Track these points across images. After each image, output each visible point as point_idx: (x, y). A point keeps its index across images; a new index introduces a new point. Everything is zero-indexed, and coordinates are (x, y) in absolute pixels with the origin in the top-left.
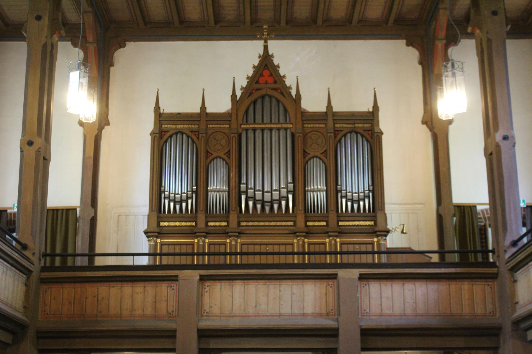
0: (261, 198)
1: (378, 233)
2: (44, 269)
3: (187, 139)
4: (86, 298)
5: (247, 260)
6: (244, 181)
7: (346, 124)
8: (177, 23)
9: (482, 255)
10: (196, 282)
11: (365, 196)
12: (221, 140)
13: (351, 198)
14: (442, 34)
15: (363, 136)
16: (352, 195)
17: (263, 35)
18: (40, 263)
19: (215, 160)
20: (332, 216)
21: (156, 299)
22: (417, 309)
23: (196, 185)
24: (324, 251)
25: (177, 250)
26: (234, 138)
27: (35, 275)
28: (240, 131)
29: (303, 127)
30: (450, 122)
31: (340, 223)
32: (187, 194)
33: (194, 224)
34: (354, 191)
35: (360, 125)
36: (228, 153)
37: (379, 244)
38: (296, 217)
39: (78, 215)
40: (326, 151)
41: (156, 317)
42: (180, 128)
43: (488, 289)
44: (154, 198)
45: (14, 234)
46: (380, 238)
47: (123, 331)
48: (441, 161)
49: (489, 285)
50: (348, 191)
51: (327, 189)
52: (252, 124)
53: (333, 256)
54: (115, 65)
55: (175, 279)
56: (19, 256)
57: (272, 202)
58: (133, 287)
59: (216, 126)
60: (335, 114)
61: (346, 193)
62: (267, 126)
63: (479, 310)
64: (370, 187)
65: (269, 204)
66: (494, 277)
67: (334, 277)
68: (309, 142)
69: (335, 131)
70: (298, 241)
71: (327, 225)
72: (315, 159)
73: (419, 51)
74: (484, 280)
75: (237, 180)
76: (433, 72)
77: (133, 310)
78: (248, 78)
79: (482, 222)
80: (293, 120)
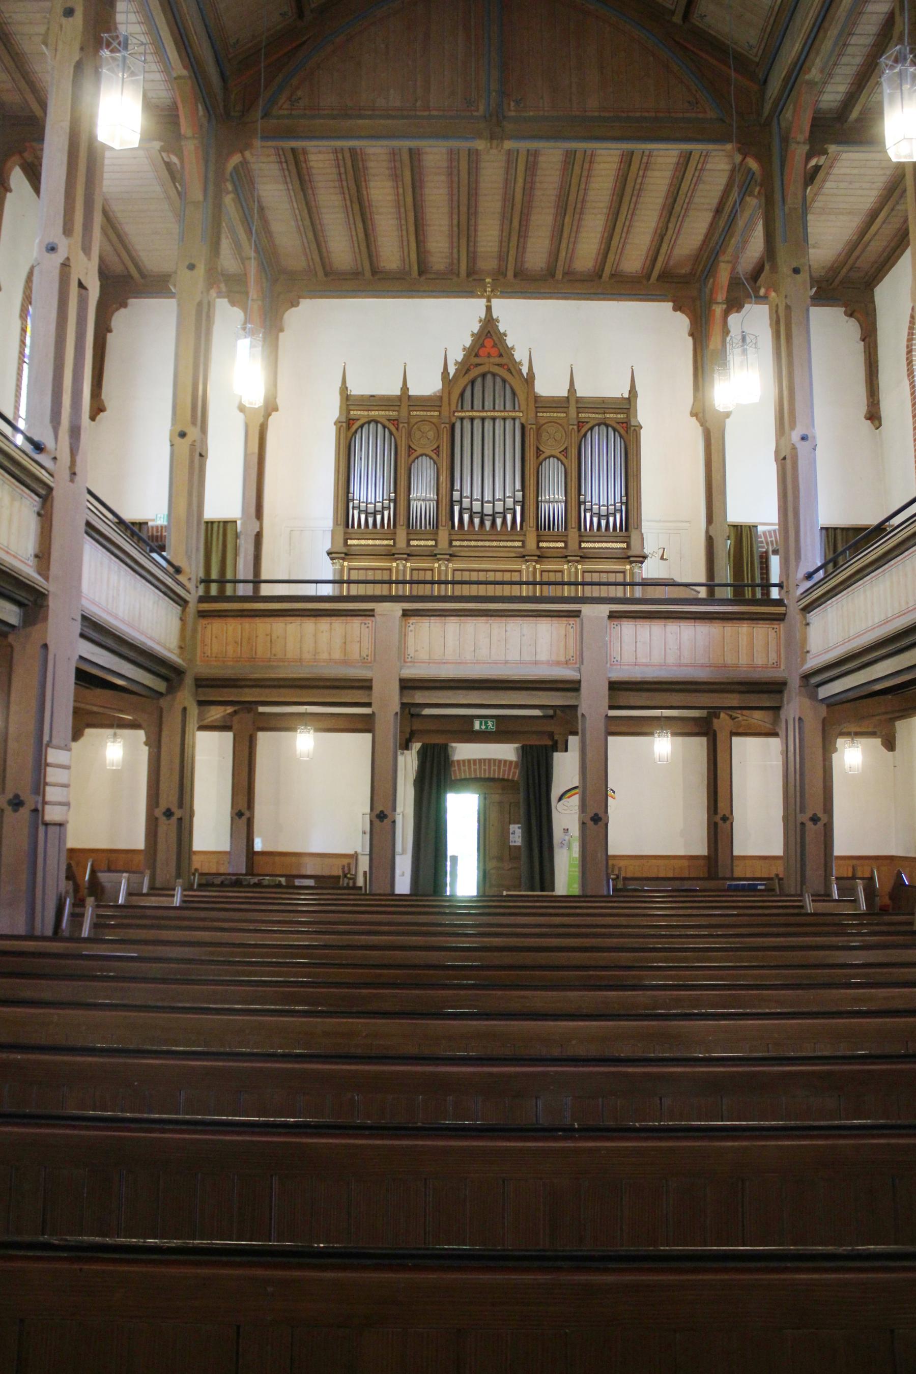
0: (479, 510)
1: (632, 559)
2: (202, 600)
3: (382, 430)
4: (257, 637)
5: (459, 590)
6: (457, 486)
7: (593, 413)
8: (368, 274)
9: (762, 590)
10: (398, 619)
11: (383, 508)
13: (597, 512)
14: (721, 296)
15: (615, 430)
16: (599, 508)
17: (486, 291)
18: (197, 591)
19: (420, 458)
20: (573, 534)
21: (345, 639)
22: (682, 658)
23: (395, 492)
24: (430, 579)
25: (370, 576)
26: (445, 429)
27: (192, 607)
28: (453, 420)
29: (537, 416)
30: (728, 415)
31: (583, 545)
32: (383, 503)
33: (391, 542)
34: (601, 504)
35: (612, 416)
36: (437, 450)
37: (632, 574)
38: (525, 535)
39: (239, 529)
40: (566, 448)
41: (345, 662)
43: (772, 634)
44: (339, 509)
45: (164, 553)
46: (634, 565)
47: (300, 679)
48: (715, 466)
49: (773, 629)
50: (594, 503)
51: (566, 500)
52: (468, 411)
53: (573, 587)
54: (285, 329)
55: (370, 614)
56: (173, 583)
57: (494, 516)
58: (316, 623)
59: (422, 413)
60: (579, 400)
61: (592, 505)
62: (489, 414)
63: (759, 661)
65: (490, 518)
66: (781, 618)
67: (576, 614)
68: (545, 436)
69: (579, 422)
70: (528, 568)
71: (566, 547)
72: (551, 459)
73: (689, 318)
74: (767, 622)
75: (449, 486)
76: (707, 346)
77: (316, 653)
78: (464, 349)
79: (763, 547)
80: (523, 408)
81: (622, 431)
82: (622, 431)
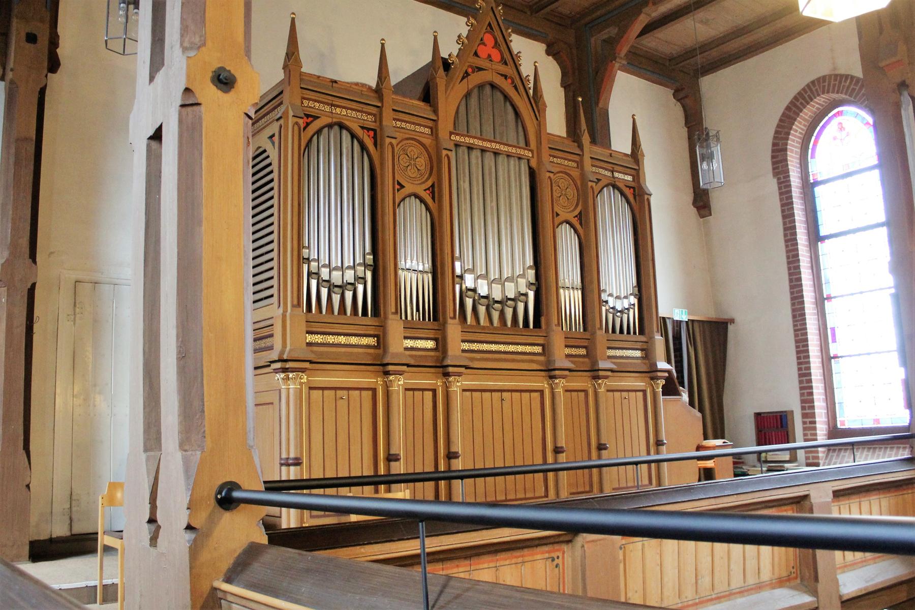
11: (357, 278)
12: (417, 158)
15: (353, 136)
50: (322, 263)
64: (368, 257)
81: (369, 143)
82: (369, 143)
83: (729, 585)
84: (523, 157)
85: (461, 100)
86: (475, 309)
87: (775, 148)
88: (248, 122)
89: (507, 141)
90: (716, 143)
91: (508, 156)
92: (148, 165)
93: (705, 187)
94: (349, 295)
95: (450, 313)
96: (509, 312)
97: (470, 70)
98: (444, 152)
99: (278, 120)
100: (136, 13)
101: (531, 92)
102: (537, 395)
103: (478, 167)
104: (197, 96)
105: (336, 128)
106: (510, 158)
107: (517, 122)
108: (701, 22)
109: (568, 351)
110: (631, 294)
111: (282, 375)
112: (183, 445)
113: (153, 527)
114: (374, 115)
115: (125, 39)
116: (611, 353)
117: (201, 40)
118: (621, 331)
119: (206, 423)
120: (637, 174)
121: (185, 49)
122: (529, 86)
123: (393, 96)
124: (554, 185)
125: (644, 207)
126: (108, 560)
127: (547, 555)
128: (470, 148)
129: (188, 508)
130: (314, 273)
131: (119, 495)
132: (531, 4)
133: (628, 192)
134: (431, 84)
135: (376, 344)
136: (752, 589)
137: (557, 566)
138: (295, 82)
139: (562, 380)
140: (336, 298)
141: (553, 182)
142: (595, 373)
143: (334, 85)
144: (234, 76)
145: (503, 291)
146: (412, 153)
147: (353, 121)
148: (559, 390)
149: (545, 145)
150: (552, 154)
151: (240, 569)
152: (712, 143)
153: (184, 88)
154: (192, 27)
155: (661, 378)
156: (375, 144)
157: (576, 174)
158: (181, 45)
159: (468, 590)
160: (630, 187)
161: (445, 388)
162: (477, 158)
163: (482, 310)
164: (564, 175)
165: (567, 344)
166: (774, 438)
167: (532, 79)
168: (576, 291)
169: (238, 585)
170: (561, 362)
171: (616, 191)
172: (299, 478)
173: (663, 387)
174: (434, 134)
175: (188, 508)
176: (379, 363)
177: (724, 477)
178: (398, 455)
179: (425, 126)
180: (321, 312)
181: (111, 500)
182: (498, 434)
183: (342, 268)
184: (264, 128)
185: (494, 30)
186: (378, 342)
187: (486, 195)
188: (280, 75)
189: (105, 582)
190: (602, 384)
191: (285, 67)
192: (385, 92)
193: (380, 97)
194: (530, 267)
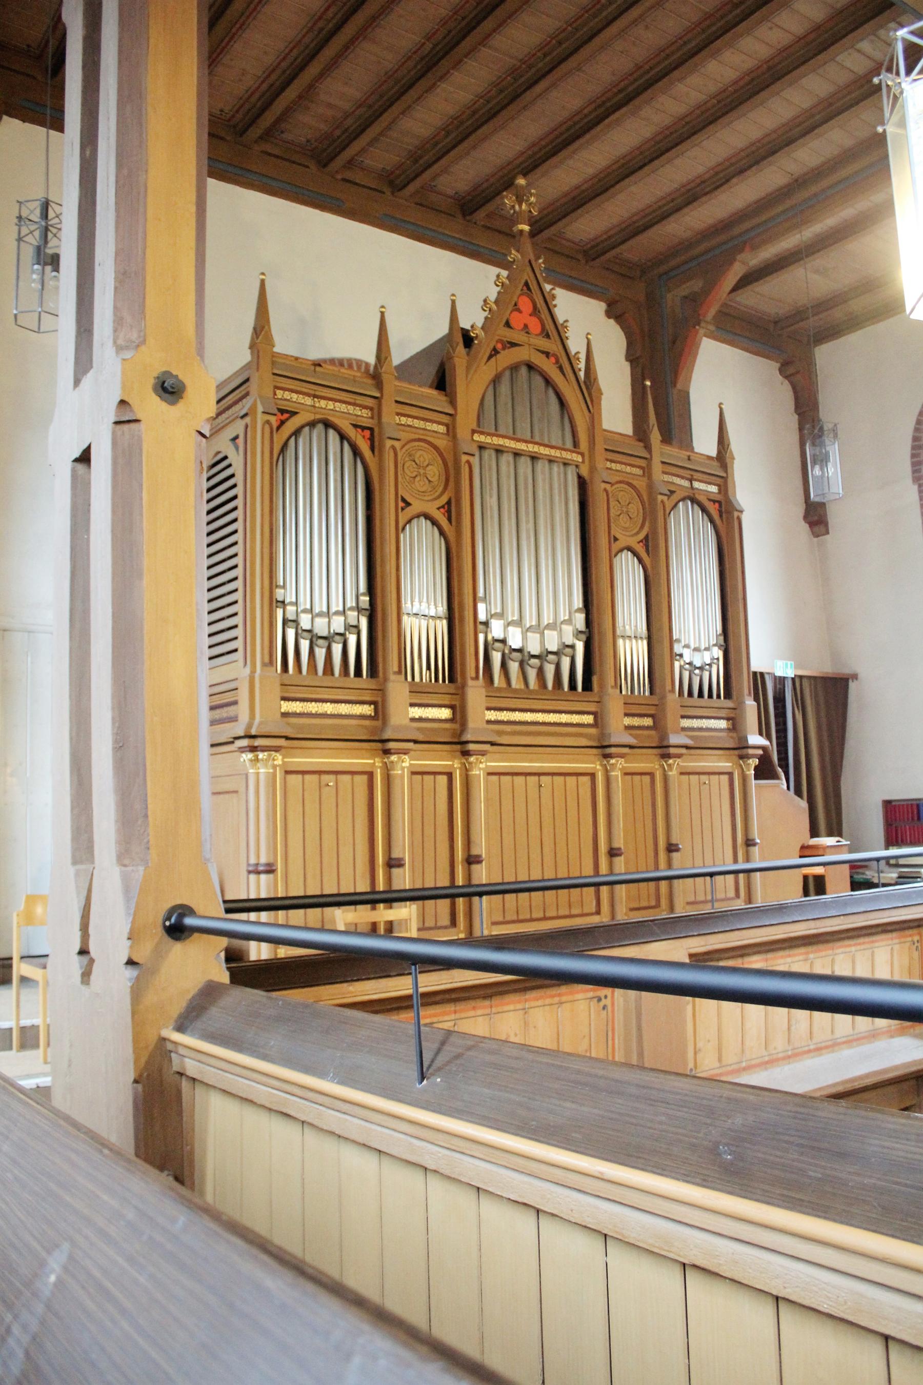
11: (348, 627)
12: (427, 466)
15: (343, 437)
19: (415, 521)
42: (325, 409)
50: (301, 608)
81: (364, 446)
82: (364, 446)
83: (832, 1032)
84: (571, 462)
85: (487, 387)
86: (504, 665)
87: (917, 443)
88: (201, 441)
89: (549, 441)
90: (832, 440)
91: (550, 461)
92: (74, 495)
93: (817, 499)
94: (337, 649)
95: (471, 672)
96: (550, 670)
97: (499, 346)
98: (464, 458)
99: (242, 417)
100: (55, 277)
101: (582, 374)
102: (586, 780)
103: (509, 477)
104: (135, 410)
105: (320, 427)
106: (552, 464)
107: (562, 417)
108: (817, 271)
109: (628, 721)
110: (714, 645)
111: (250, 756)
112: (123, 857)
113: (85, 959)
114: (371, 409)
115: (40, 313)
116: (686, 723)
117: (139, 337)
118: (701, 695)
119: (151, 830)
120: (724, 483)
121: (119, 349)
122: (579, 366)
123: (397, 383)
124: (611, 500)
125: (733, 527)
126: (25, 993)
127: (591, 994)
128: (499, 451)
129: (129, 939)
130: (291, 621)
131: (39, 910)
132: (585, 248)
133: (713, 509)
134: (447, 367)
135: (373, 714)
136: (863, 1038)
137: (604, 1007)
138: (265, 365)
139: (621, 761)
140: (320, 653)
141: (610, 495)
142: (664, 751)
143: (318, 369)
144: (183, 383)
145: (542, 642)
146: (422, 459)
147: (344, 418)
148: (616, 774)
149: (600, 446)
150: (609, 458)
151: (194, 1014)
152: (827, 440)
153: (119, 400)
154: (128, 319)
155: (753, 756)
156: (372, 448)
157: (641, 484)
158: (115, 342)
159: (469, 1048)
160: (714, 501)
161: (464, 772)
162: (508, 463)
163: (514, 667)
164: (626, 486)
165: (627, 712)
166: (908, 833)
167: (583, 357)
168: (640, 641)
169: (192, 1035)
170: (618, 736)
171: (696, 506)
172: (272, 896)
173: (756, 769)
174: (451, 434)
175: (129, 939)
176: (377, 739)
177: (838, 883)
178: (402, 859)
179: (439, 423)
180: (300, 671)
181: (29, 918)
182: (534, 831)
183: (328, 614)
184: (223, 427)
185: (533, 291)
186: (376, 710)
187: (520, 516)
188: (246, 357)
189: (26, 1022)
190: (674, 764)
191: (252, 347)
192: (385, 377)
193: (379, 385)
194: (578, 610)
